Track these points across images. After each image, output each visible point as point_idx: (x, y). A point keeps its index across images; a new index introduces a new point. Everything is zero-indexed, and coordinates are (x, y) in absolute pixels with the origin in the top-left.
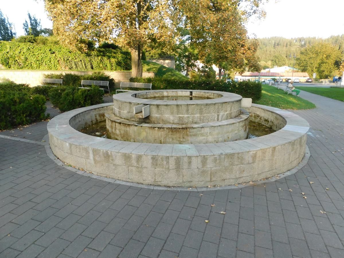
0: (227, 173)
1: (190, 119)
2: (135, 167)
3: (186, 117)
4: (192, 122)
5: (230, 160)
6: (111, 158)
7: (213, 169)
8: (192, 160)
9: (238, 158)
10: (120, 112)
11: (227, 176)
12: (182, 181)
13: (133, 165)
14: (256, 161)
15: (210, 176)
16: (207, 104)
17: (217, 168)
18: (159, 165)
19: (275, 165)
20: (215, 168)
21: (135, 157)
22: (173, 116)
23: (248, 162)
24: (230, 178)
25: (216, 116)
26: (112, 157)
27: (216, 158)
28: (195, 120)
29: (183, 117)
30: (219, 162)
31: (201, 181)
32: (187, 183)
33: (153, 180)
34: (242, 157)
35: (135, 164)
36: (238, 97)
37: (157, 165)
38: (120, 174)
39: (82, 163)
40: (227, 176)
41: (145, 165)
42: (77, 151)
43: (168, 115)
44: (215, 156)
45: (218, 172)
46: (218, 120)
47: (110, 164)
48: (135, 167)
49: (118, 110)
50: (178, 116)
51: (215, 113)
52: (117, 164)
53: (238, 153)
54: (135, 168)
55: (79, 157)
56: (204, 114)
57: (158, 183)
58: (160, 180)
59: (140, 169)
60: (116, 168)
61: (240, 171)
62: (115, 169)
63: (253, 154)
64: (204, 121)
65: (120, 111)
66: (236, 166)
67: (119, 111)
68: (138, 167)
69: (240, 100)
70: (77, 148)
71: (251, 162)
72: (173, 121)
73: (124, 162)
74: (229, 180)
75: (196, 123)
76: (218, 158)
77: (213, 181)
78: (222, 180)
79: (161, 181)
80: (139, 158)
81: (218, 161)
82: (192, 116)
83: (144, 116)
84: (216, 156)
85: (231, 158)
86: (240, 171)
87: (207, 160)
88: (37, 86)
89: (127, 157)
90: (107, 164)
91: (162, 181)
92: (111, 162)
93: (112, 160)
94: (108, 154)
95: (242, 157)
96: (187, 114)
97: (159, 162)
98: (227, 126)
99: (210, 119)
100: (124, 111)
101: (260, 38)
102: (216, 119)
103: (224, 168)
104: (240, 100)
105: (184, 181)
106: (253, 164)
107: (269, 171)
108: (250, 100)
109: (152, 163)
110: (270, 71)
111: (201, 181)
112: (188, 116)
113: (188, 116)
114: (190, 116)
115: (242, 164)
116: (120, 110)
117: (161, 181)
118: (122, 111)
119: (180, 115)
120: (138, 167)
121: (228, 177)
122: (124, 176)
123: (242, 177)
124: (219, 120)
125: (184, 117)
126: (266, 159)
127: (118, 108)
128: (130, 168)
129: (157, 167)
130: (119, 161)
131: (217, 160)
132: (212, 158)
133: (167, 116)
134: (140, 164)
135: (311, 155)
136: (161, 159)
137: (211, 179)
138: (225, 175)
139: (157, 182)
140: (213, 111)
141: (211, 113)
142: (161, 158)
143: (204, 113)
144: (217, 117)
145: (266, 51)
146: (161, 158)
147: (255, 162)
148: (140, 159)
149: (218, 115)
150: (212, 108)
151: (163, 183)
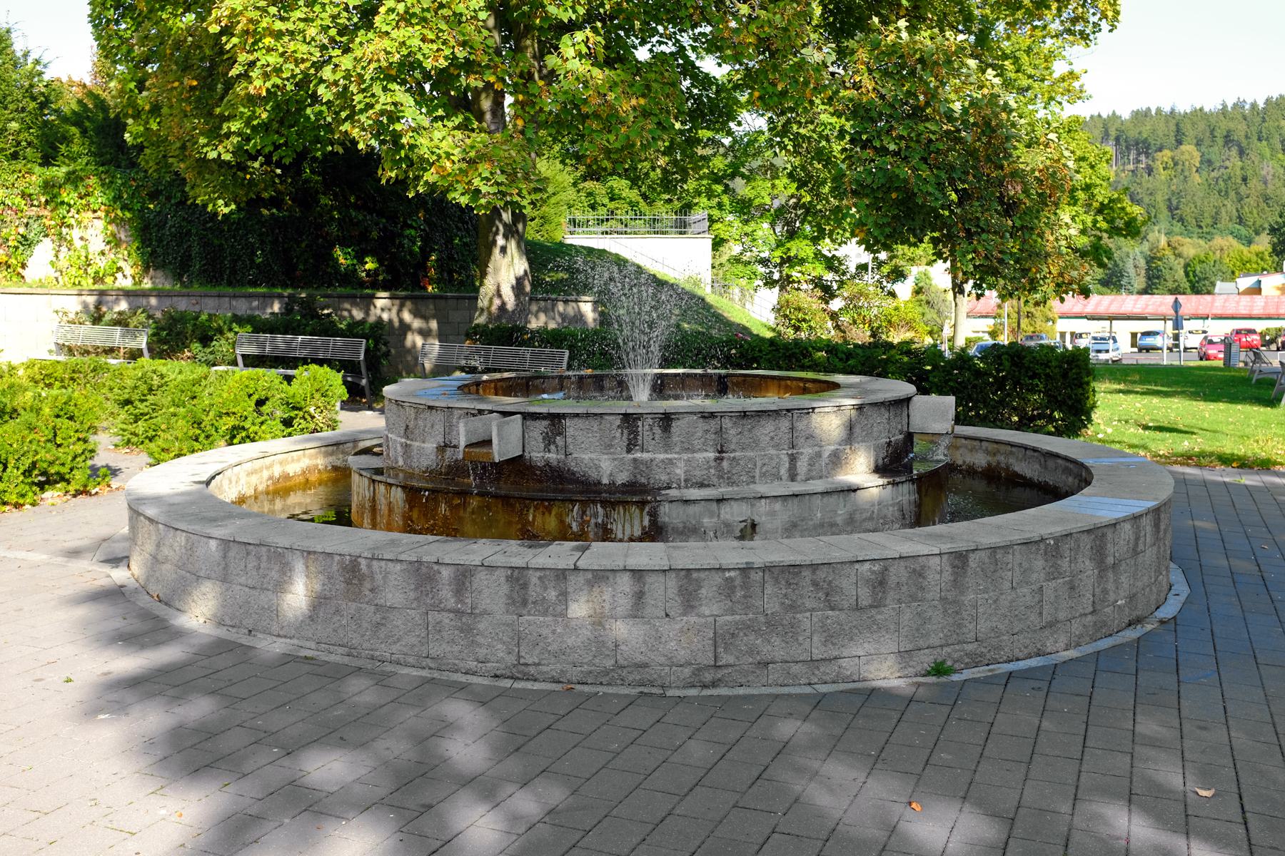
0: (776, 641)
1: (678, 471)
2: (450, 611)
3: (663, 461)
4: (686, 481)
5: (784, 591)
6: (367, 585)
7: (721, 620)
8: (647, 586)
9: (815, 584)
10: (406, 447)
11: (775, 648)
12: (613, 662)
13: (442, 606)
14: (888, 602)
15: (713, 648)
16: (744, 415)
17: (738, 617)
18: (534, 603)
19: (971, 626)
20: (729, 618)
21: (452, 575)
22: (610, 456)
23: (853, 601)
24: (789, 659)
25: (786, 459)
26: (372, 578)
27: (731, 579)
28: (698, 474)
29: (652, 461)
30: (745, 597)
31: (681, 666)
32: (629, 669)
33: (511, 659)
34: (830, 582)
35: (451, 603)
36: (904, 388)
37: (524, 603)
38: (399, 640)
39: (263, 608)
40: (775, 648)
41: (485, 603)
42: (250, 566)
43: (593, 456)
44: (727, 575)
45: (741, 634)
46: (793, 477)
47: (364, 606)
48: (450, 611)
49: (403, 440)
50: (630, 456)
51: (777, 446)
52: (388, 604)
53: (814, 567)
54: (451, 615)
55: (254, 588)
56: (734, 451)
57: (526, 669)
58: (537, 661)
59: (467, 618)
60: (384, 621)
61: (825, 634)
62: (382, 625)
63: (873, 572)
64: (735, 477)
65: (410, 445)
66: (808, 614)
67: (406, 445)
68: (457, 612)
69: (908, 400)
70: (248, 554)
71: (865, 603)
72: (611, 475)
73: (412, 595)
74: (785, 665)
75: (702, 485)
76: (738, 582)
77: (727, 666)
78: (759, 663)
79: (539, 664)
80: (466, 577)
81: (739, 593)
82: (685, 456)
83: (500, 456)
84: (732, 574)
85: (789, 584)
86: (825, 634)
87: (700, 587)
88: (1125, 114)
89: (423, 575)
90: (353, 605)
91: (543, 662)
92: (367, 599)
93: (372, 590)
94: (359, 570)
95: (830, 582)
96: (666, 452)
97: (534, 591)
98: (826, 499)
99: (757, 471)
100: (424, 442)
101: (1206, 109)
102: (784, 472)
103: (762, 619)
104: (908, 400)
105: (621, 662)
106: (873, 612)
107: (948, 645)
108: (949, 402)
109: (509, 597)
110: (1263, 286)
111: (681, 666)
112: (669, 456)
113: (669, 456)
114: (676, 456)
115: (833, 609)
116: (408, 442)
117: (539, 664)
118: (416, 444)
119: (638, 455)
120: (457, 612)
121: (779, 654)
122: (413, 646)
123: (836, 658)
124: (799, 478)
125: (654, 463)
126: (929, 596)
127: (402, 432)
128: (433, 617)
129: (524, 612)
130: (395, 592)
131: (735, 587)
132: (717, 578)
133: (586, 457)
134: (469, 601)
135: (1174, 618)
136: (538, 582)
137: (716, 657)
138: (770, 648)
139: (526, 665)
140: (772, 438)
141: (764, 449)
142: (540, 578)
143: (733, 447)
144: (787, 465)
145: (1245, 179)
146: (540, 578)
147: (885, 606)
148: (468, 584)
149: (793, 459)
150: (766, 429)
151: (545, 669)
